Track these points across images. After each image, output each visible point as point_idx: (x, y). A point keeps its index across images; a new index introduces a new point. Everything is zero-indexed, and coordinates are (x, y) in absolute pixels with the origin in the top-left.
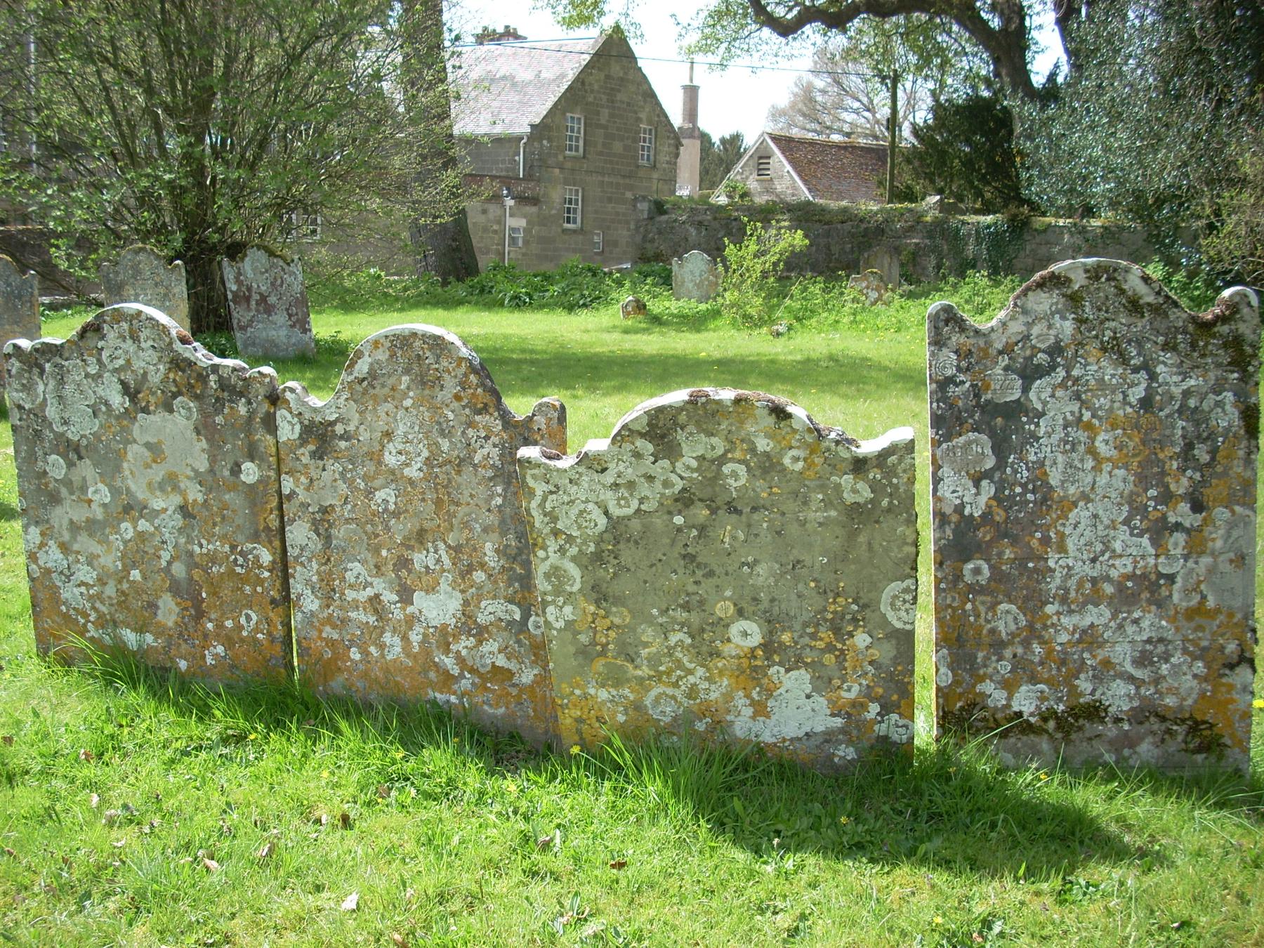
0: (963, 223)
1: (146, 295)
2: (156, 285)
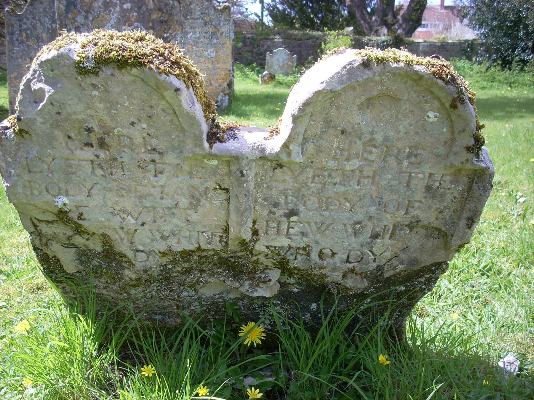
1: (195, 33)
2: (206, 24)
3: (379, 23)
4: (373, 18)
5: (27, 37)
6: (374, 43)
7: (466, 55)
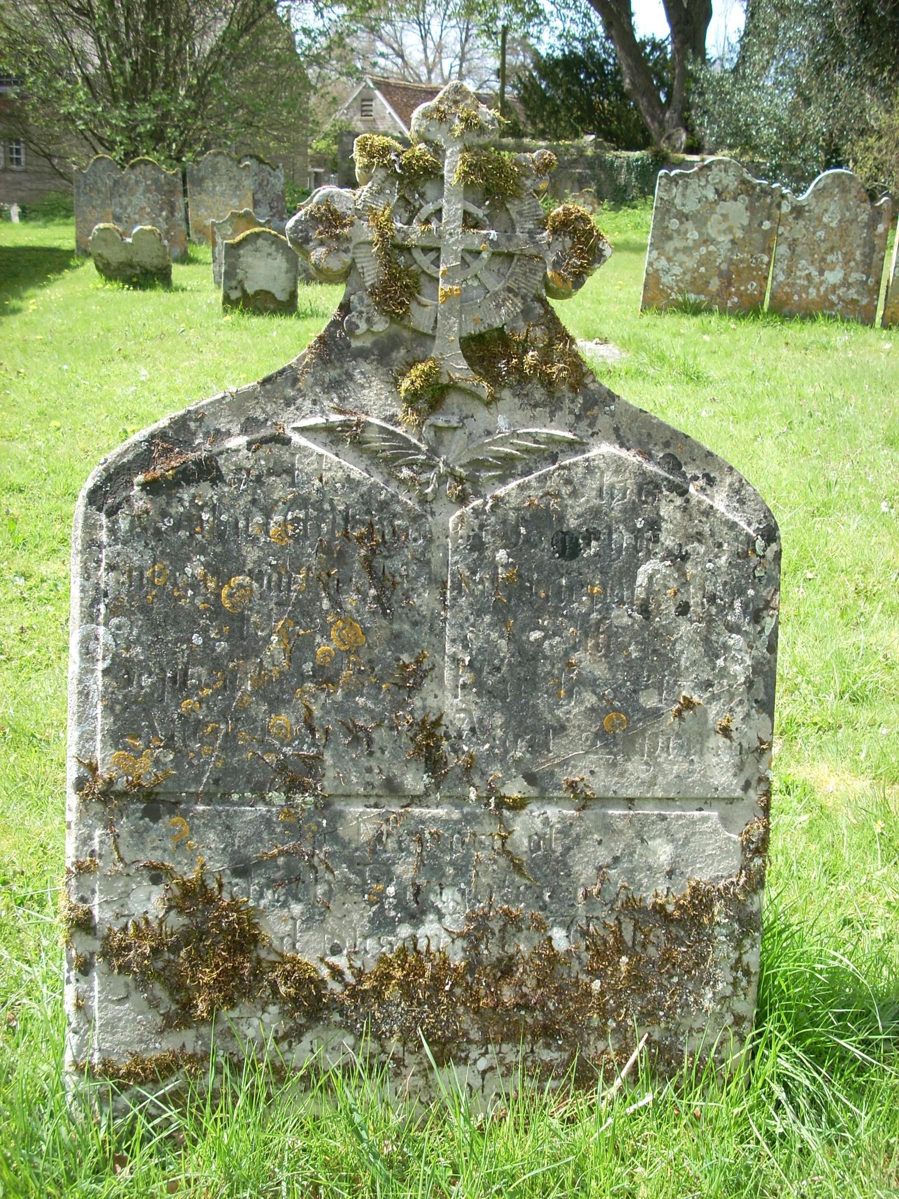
0: (617, 157)
4: (667, 115)
5: (91, 190)
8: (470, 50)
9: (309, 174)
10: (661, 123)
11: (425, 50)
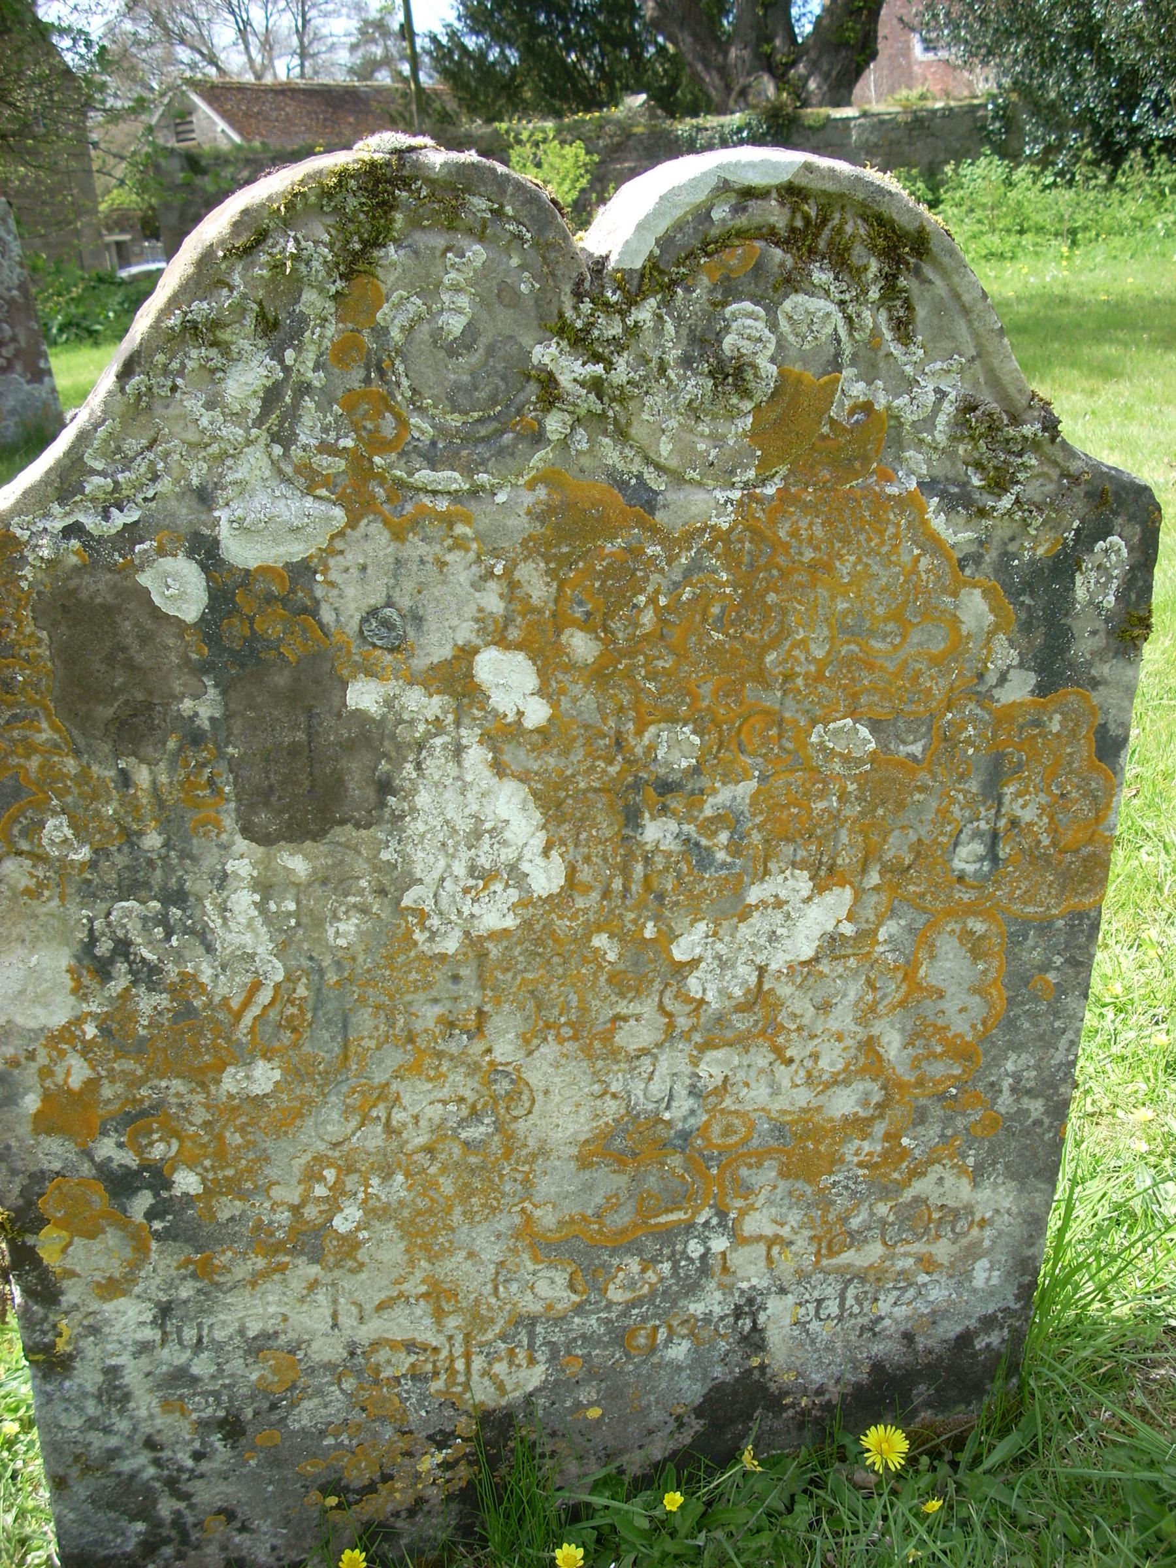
0: (699, 129)
3: (748, 65)
6: (712, 138)
7: (991, 142)
8: (311, 43)
9: (107, 246)
10: (723, 71)
11: (247, 48)
